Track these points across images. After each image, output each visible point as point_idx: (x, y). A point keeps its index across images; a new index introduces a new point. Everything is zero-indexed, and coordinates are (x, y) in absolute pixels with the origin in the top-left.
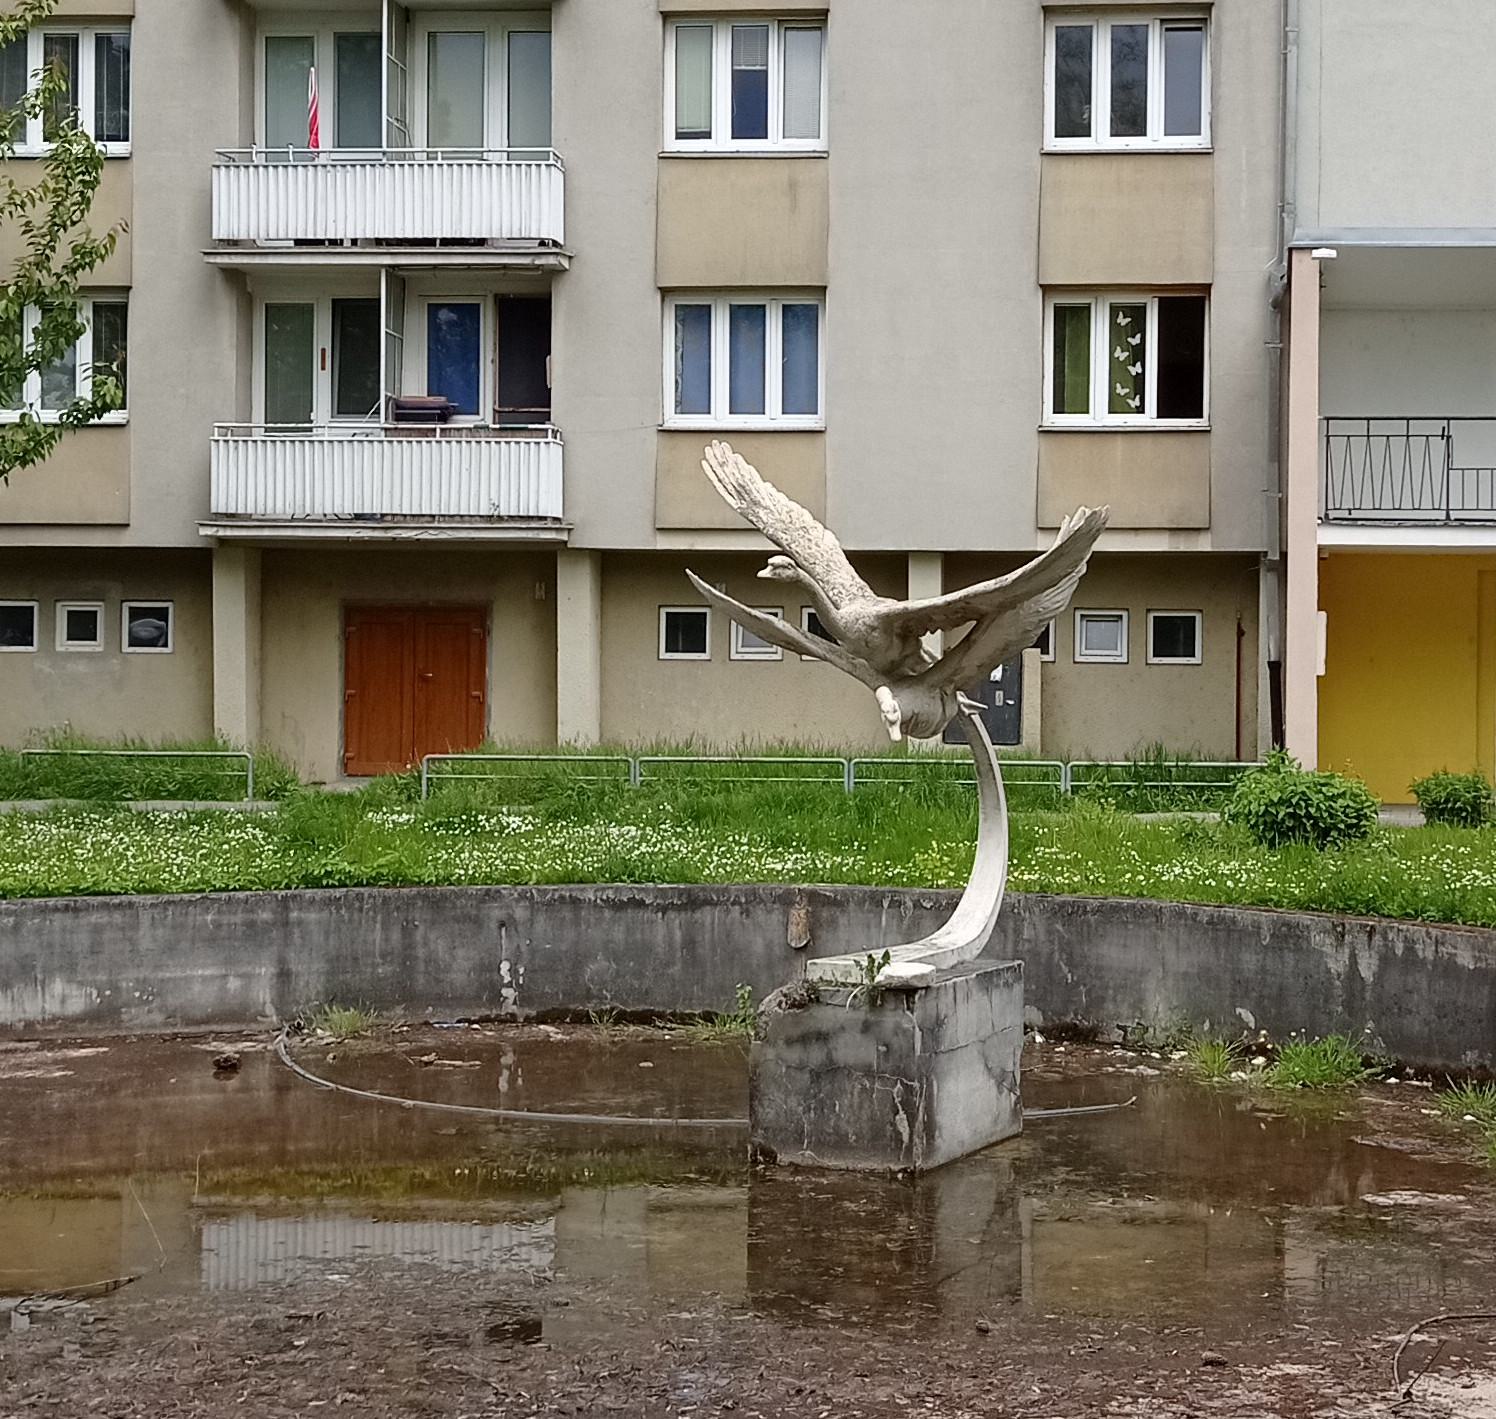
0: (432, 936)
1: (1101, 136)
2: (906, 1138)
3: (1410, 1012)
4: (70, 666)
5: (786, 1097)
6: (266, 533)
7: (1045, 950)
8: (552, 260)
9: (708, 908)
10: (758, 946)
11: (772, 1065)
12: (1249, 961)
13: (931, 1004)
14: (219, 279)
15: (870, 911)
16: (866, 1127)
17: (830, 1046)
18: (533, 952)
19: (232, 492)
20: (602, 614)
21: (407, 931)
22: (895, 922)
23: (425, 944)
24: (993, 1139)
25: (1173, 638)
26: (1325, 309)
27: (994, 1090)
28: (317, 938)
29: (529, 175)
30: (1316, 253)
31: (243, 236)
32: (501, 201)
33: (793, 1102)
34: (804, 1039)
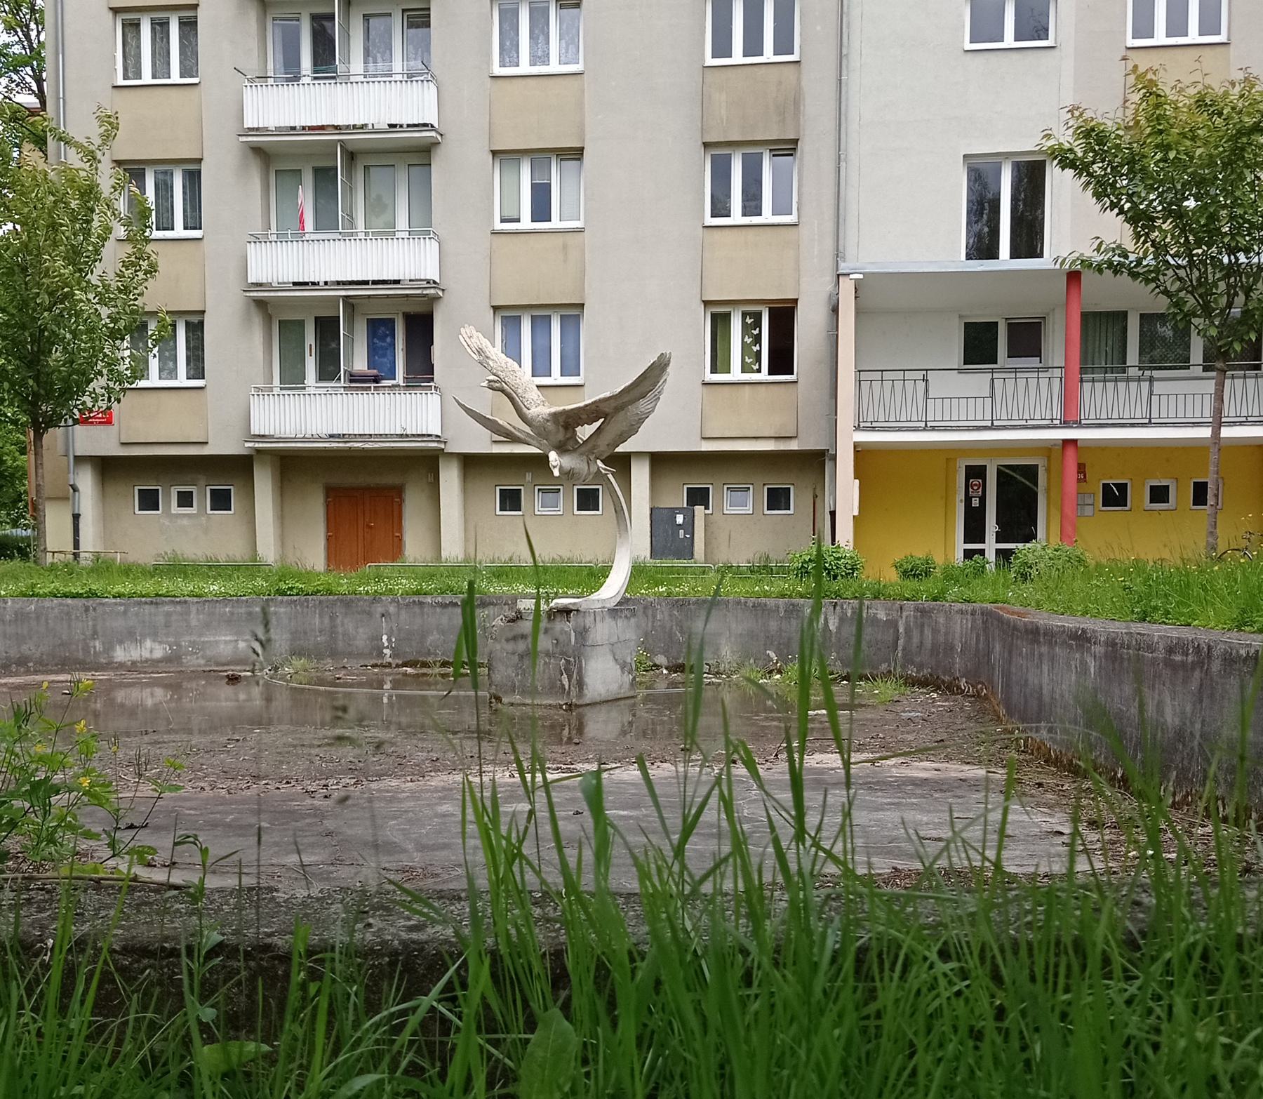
0: (346, 621)
1: (737, 217)
2: (567, 687)
4: (179, 521)
6: (281, 445)
7: (668, 625)
8: (432, 291)
12: (773, 625)
13: (580, 620)
14: (253, 304)
16: (547, 682)
18: (399, 630)
19: (262, 423)
20: (465, 490)
21: (333, 618)
23: (343, 625)
24: (619, 696)
25: (778, 499)
26: (858, 312)
27: (619, 671)
28: (285, 621)
29: (419, 244)
30: (851, 276)
31: (264, 281)
32: (404, 253)
33: (510, 671)
34: (515, 638)
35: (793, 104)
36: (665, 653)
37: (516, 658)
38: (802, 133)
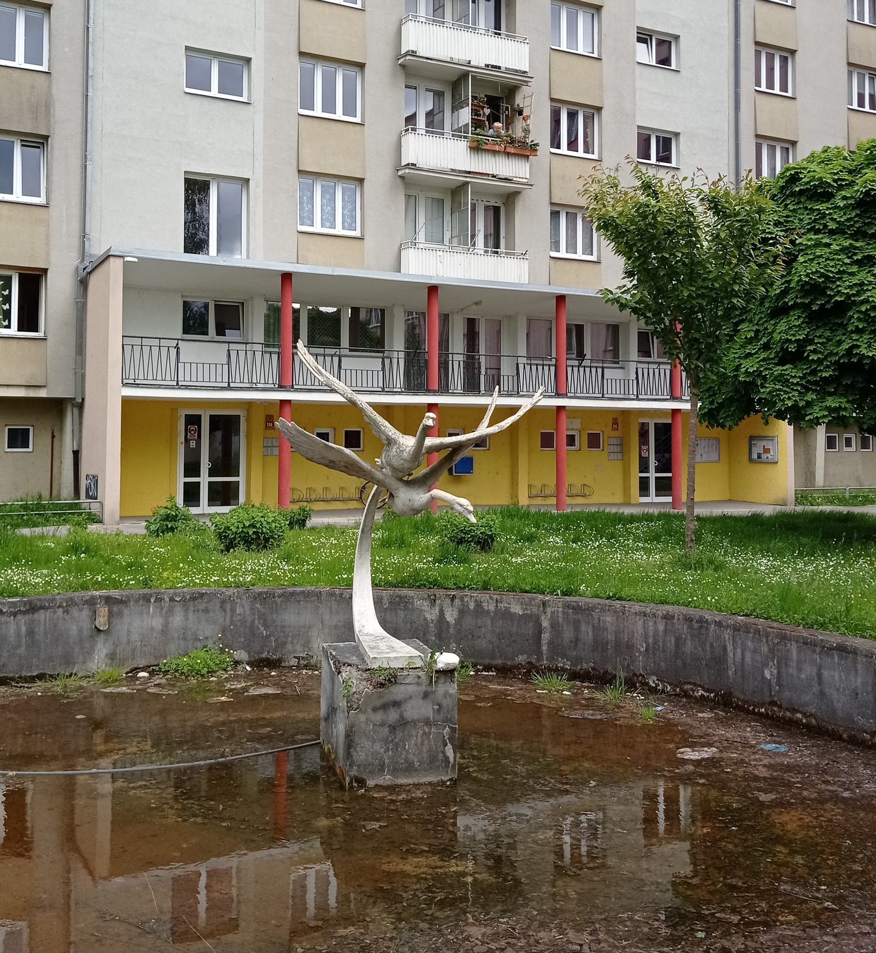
3: (480, 637)
5: (373, 744)
7: (249, 619)
9: (43, 611)
10: (74, 630)
11: (363, 726)
15: (142, 605)
16: (425, 756)
17: (402, 709)
22: (158, 610)
33: (378, 747)
34: (385, 707)
35: (46, 106)
36: (246, 647)
37: (387, 729)
38: (52, 131)
